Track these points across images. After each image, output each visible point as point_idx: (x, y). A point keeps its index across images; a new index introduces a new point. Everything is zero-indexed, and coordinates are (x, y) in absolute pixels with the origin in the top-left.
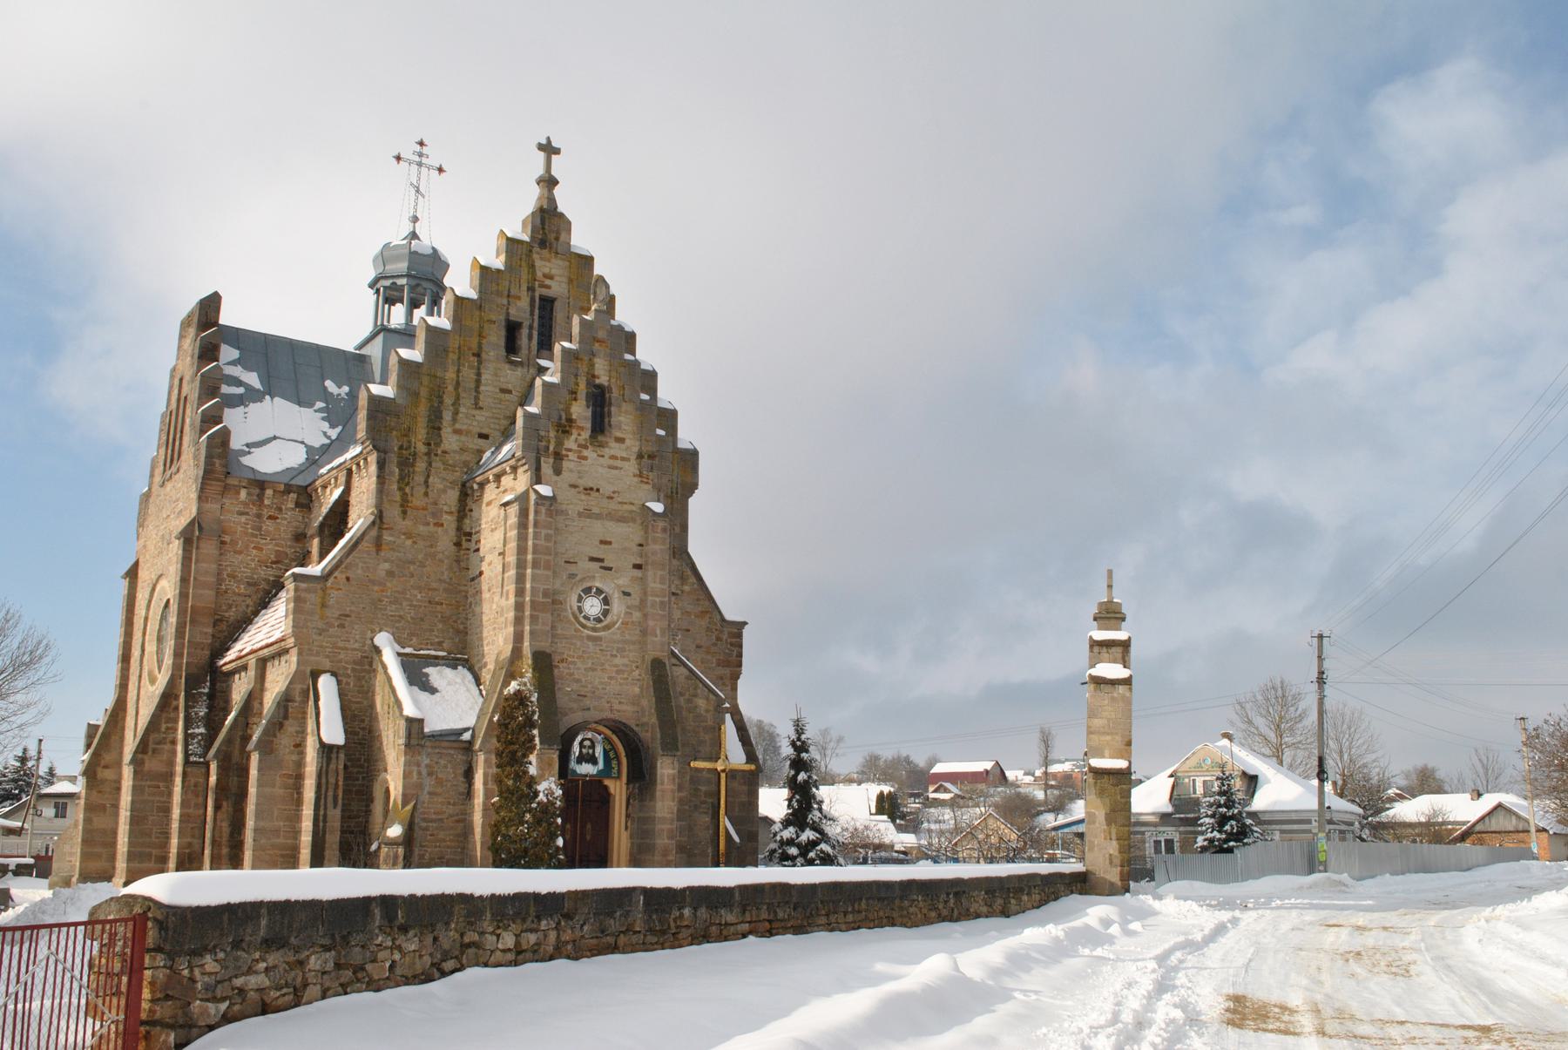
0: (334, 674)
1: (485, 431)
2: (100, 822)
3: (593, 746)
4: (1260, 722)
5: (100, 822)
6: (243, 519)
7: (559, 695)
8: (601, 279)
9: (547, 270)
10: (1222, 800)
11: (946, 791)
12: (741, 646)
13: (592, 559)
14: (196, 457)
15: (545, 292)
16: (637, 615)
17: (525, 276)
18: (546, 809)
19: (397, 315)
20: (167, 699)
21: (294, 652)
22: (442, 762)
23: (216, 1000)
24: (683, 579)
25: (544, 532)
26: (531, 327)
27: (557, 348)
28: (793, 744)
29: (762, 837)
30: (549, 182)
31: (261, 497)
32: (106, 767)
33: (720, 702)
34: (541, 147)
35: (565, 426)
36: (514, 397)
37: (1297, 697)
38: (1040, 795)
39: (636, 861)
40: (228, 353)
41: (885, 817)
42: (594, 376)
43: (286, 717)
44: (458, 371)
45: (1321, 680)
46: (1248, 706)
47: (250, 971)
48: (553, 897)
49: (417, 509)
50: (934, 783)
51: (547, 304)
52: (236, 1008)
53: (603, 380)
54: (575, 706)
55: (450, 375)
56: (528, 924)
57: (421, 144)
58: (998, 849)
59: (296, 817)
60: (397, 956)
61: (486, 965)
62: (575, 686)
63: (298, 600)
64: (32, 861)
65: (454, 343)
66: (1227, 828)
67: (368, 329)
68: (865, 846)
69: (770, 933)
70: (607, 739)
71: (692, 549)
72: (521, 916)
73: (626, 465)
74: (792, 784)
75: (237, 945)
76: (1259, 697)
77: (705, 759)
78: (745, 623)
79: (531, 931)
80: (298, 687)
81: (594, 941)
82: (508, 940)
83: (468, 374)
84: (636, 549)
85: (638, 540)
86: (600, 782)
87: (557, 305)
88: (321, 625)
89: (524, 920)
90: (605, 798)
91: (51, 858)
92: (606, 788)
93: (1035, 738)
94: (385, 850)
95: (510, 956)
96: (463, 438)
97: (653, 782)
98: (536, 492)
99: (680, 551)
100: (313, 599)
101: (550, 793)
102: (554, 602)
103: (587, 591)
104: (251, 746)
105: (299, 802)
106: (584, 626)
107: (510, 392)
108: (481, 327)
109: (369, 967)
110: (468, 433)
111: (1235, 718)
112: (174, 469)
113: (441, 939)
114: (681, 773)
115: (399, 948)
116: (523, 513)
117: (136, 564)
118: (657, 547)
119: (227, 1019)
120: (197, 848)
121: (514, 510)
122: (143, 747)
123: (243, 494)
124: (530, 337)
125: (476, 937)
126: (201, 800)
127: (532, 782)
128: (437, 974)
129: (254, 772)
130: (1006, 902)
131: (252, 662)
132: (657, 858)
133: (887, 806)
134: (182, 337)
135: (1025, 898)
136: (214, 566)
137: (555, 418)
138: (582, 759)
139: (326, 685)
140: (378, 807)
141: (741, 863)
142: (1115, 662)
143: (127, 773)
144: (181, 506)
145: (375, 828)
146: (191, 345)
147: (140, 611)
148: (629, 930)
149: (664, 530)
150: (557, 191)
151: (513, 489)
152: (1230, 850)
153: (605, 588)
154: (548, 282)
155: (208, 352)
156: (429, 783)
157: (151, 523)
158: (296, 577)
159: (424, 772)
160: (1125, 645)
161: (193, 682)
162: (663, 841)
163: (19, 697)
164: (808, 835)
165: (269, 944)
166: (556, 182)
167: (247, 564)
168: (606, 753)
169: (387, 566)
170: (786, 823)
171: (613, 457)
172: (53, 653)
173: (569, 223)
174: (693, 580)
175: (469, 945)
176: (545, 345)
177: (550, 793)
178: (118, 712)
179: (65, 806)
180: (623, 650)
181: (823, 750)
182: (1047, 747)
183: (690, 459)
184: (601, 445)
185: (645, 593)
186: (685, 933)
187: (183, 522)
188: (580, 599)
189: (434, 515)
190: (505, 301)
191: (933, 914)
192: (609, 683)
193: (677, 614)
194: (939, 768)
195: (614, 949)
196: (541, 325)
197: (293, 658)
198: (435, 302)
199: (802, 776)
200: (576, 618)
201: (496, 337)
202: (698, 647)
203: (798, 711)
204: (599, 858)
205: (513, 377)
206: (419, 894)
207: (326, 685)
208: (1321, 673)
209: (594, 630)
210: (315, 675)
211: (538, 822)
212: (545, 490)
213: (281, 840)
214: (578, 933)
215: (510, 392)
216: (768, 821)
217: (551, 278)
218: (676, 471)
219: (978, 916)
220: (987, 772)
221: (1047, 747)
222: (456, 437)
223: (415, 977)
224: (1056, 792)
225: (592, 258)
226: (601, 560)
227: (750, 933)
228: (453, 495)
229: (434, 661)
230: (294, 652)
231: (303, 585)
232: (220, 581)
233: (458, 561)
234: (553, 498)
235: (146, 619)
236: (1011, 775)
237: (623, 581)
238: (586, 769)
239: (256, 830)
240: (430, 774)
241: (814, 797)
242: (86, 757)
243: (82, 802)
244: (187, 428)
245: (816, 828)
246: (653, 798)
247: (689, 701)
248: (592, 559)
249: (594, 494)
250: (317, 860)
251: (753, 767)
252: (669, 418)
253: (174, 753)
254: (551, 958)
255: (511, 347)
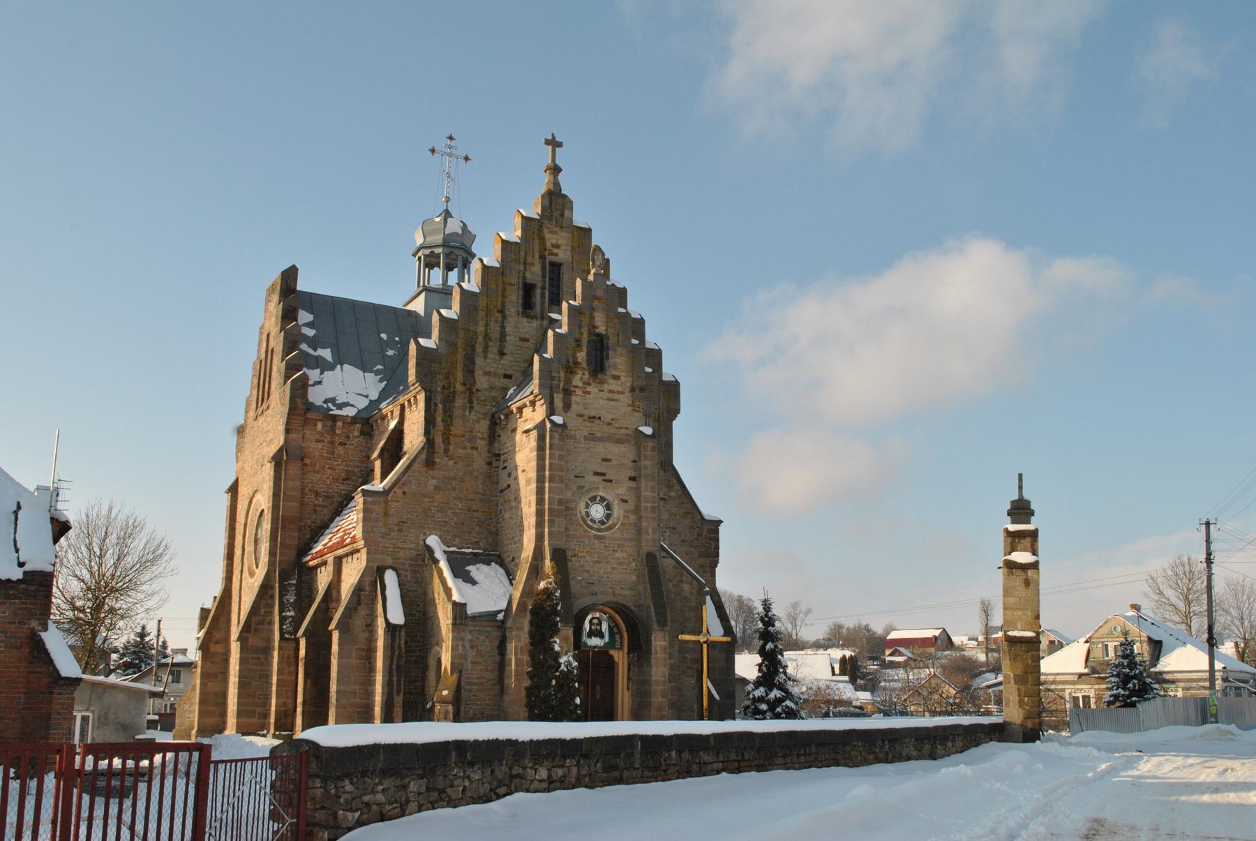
0: (394, 569)
1: (509, 372)
2: (213, 686)
3: (600, 624)
4: (1170, 593)
5: (213, 686)
6: (320, 445)
7: (572, 583)
8: (598, 248)
9: (554, 241)
10: (1125, 662)
11: (901, 654)
12: (718, 540)
13: (596, 474)
14: (281, 399)
15: (553, 258)
16: (633, 518)
17: (537, 247)
18: (567, 675)
19: (436, 278)
20: (265, 588)
21: (364, 551)
22: (482, 638)
23: (353, 810)
24: (669, 487)
25: (557, 453)
26: (543, 288)
27: (565, 305)
28: (762, 620)
29: (739, 695)
30: (555, 170)
31: (333, 428)
32: (217, 643)
33: (701, 586)
34: (547, 142)
35: (571, 368)
36: (531, 344)
37: (844, 657)
38: (982, 657)
39: (637, 716)
40: (304, 317)
41: (846, 678)
42: (594, 327)
43: (359, 603)
44: (487, 325)
45: (1209, 561)
46: (1159, 580)
47: (373, 792)
48: (574, 742)
49: (456, 436)
50: (889, 648)
51: (556, 267)
52: (365, 816)
53: (601, 329)
54: (585, 591)
55: (481, 328)
56: (557, 762)
57: (451, 138)
58: (939, 703)
59: (370, 682)
60: (467, 783)
61: (528, 791)
62: (585, 575)
63: (366, 511)
64: (157, 717)
65: (482, 303)
66: (1130, 685)
67: (415, 290)
68: (828, 702)
69: (738, 770)
70: (611, 618)
71: (678, 462)
72: (551, 756)
73: (621, 396)
74: (762, 652)
75: (364, 774)
76: (1170, 573)
77: (690, 633)
78: (721, 522)
79: (559, 767)
80: (368, 579)
81: (605, 775)
82: (543, 773)
83: (495, 328)
84: (631, 464)
85: (632, 457)
86: (607, 652)
87: (564, 269)
88: (383, 530)
89: (554, 759)
90: (611, 665)
91: (174, 715)
92: (611, 656)
93: (977, 608)
94: (438, 707)
95: (545, 785)
96: (492, 379)
97: (649, 651)
98: (551, 421)
99: (666, 465)
100: (378, 509)
101: (569, 664)
102: (567, 509)
103: (593, 499)
104: (332, 626)
105: (371, 669)
106: (591, 527)
107: (527, 340)
108: (504, 289)
109: (448, 790)
110: (495, 374)
111: (1148, 590)
112: (264, 406)
113: (499, 770)
114: (671, 644)
115: (468, 777)
116: (541, 439)
117: (236, 483)
118: (648, 463)
119: (360, 823)
120: (291, 706)
121: (534, 434)
122: (247, 628)
123: (320, 426)
124: (543, 295)
125: (521, 771)
126: (292, 668)
127: (557, 656)
128: (494, 797)
129: (335, 647)
130: (934, 748)
131: (330, 558)
132: (653, 712)
133: (850, 668)
134: (268, 301)
135: (950, 744)
136: (298, 483)
137: (564, 362)
138: (591, 634)
139: (390, 578)
140: (432, 675)
141: (721, 718)
142: (1025, 550)
143: (235, 648)
144: (271, 435)
145: (430, 690)
146: (275, 308)
147: (240, 519)
148: (631, 767)
149: (653, 449)
150: (561, 177)
151: (532, 419)
152: (1133, 705)
153: (607, 497)
154: (555, 251)
155: (288, 315)
156: (471, 654)
157: (248, 448)
158: (365, 493)
159: (468, 646)
160: (1034, 534)
161: (284, 576)
162: (657, 699)
163: (145, 587)
164: (775, 694)
165: (384, 773)
166: (560, 170)
167: (324, 480)
168: (610, 629)
169: (434, 482)
170: (757, 684)
171: (611, 391)
172: (170, 552)
173: (571, 202)
174: (677, 487)
175: (516, 776)
176: (556, 302)
177: (569, 664)
178: (225, 600)
179: (179, 673)
180: (623, 546)
181: (793, 620)
182: (987, 615)
183: (673, 389)
184: (601, 382)
185: (639, 500)
186: (673, 770)
187: (273, 449)
188: (587, 506)
189: (470, 440)
190: (522, 268)
191: (871, 757)
192: (611, 571)
193: (665, 516)
194: (894, 635)
195: (620, 781)
196: (551, 285)
197: (363, 555)
198: (466, 265)
199: (770, 646)
200: (585, 521)
201: (514, 298)
202: (683, 541)
203: (766, 593)
204: (609, 715)
205: (529, 327)
206: (481, 739)
207: (390, 578)
208: (1209, 554)
209: (599, 530)
210: (381, 571)
211: (560, 686)
212: (558, 419)
213: (358, 700)
214: (593, 769)
215: (527, 340)
216: (744, 681)
217: (558, 247)
218: (662, 400)
219: (909, 758)
220: (936, 638)
221: (987, 615)
222: (486, 378)
223: (479, 798)
224: (995, 655)
225: (590, 230)
226: (604, 474)
227: (723, 770)
228: (484, 425)
229: (475, 559)
230: (364, 552)
231: (370, 499)
232: (303, 494)
233: (490, 477)
234: (564, 426)
235: (245, 525)
236: (956, 640)
237: (621, 490)
238: (595, 642)
239: (338, 692)
240: (472, 647)
241: (780, 662)
242: (201, 634)
243: (199, 670)
244: (274, 374)
245: (781, 687)
246: (649, 664)
247: (676, 586)
248: (596, 474)
249: (597, 422)
250: (388, 718)
251: (729, 639)
252: (655, 357)
253: (272, 632)
254: (573, 788)
255: (527, 304)
